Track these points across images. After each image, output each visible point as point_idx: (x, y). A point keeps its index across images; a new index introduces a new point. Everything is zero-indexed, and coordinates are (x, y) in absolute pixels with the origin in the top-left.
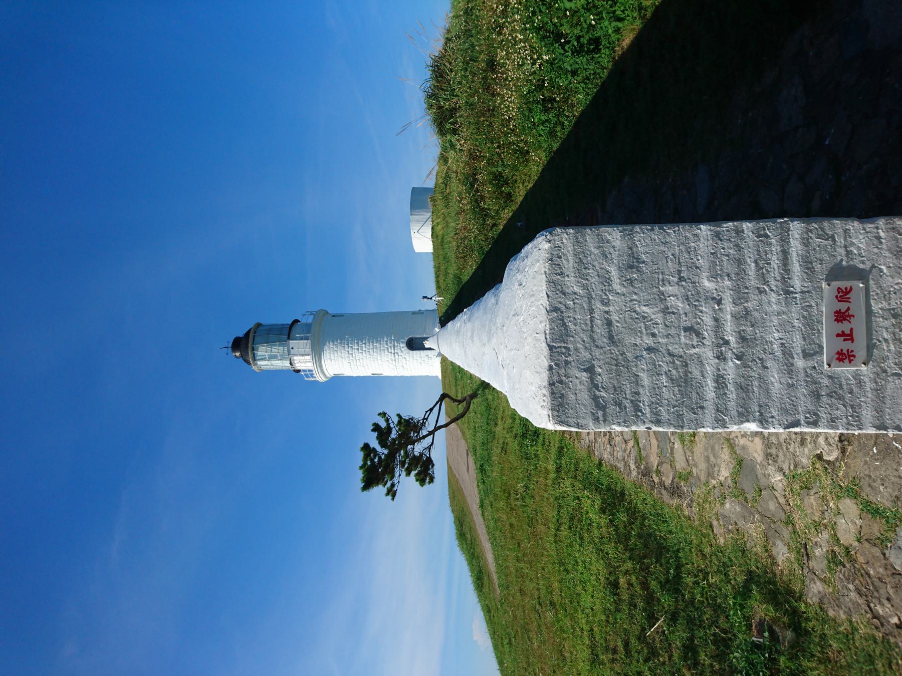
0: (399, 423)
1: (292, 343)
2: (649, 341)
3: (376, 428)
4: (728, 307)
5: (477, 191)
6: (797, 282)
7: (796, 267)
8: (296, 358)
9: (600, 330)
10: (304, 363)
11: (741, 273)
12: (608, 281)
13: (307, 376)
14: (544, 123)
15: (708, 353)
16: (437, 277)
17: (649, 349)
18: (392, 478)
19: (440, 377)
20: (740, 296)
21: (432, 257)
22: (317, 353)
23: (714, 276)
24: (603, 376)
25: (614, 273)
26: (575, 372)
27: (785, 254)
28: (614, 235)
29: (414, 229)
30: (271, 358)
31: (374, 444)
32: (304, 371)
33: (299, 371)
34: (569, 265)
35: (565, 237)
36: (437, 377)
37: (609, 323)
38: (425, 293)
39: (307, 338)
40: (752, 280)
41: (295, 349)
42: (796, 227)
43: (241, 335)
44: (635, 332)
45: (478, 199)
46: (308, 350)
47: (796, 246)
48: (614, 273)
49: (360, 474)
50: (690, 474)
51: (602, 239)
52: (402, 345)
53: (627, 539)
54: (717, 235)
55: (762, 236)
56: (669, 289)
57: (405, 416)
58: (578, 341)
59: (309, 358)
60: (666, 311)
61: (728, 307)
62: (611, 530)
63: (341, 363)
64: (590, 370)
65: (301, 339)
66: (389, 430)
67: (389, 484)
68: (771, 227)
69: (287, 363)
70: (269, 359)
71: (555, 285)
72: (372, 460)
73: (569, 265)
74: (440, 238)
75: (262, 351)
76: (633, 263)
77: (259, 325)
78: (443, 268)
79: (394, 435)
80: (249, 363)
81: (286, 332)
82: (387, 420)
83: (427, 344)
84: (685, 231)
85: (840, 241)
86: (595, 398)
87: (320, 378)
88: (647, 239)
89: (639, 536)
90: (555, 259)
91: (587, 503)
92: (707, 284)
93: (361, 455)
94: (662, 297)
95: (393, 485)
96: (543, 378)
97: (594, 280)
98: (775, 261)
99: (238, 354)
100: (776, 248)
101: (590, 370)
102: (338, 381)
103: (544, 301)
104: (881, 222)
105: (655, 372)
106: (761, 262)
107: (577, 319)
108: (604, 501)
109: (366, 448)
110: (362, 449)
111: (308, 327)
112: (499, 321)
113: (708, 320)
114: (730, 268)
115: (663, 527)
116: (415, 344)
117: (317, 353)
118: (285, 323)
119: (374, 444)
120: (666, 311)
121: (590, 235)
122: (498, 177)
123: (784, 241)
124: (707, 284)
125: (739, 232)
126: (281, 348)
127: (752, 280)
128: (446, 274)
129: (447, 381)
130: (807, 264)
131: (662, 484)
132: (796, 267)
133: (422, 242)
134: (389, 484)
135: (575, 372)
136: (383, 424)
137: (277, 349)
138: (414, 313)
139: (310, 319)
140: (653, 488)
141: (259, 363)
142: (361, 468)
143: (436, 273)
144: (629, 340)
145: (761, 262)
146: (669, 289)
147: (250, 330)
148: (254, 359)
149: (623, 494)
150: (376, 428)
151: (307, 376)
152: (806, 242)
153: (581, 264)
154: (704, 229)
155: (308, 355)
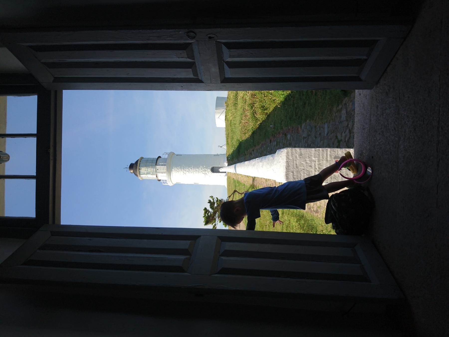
0: (217, 201)
1: (158, 167)
2: (303, 168)
3: (210, 202)
4: (317, 163)
5: (254, 110)
6: (329, 159)
7: (329, 156)
8: (158, 174)
9: (295, 166)
10: (162, 176)
11: (319, 157)
12: (296, 157)
13: (164, 183)
14: (282, 95)
15: (313, 170)
16: (227, 139)
17: (303, 169)
18: (215, 222)
19: (226, 186)
20: (319, 161)
21: (225, 130)
22: (169, 171)
23: (315, 157)
24: (295, 174)
25: (298, 156)
26: (290, 173)
27: (327, 154)
28: (298, 149)
29: (217, 116)
30: (148, 173)
31: (209, 208)
32: (163, 180)
33: (160, 180)
34: (290, 154)
35: (289, 149)
36: (224, 186)
37: (296, 164)
38: (220, 146)
39: (165, 165)
40: (321, 158)
41: (159, 170)
42: (329, 150)
43: (134, 162)
44: (301, 166)
45: (254, 113)
46: (165, 171)
47: (329, 153)
48: (298, 156)
49: (203, 219)
50: (320, 206)
51: (296, 150)
52: (209, 170)
53: (303, 227)
54: (315, 150)
55: (323, 151)
56: (307, 159)
57: (219, 199)
58: (291, 168)
59: (165, 174)
60: (306, 163)
61: (317, 163)
62: (299, 226)
63: (180, 177)
64: (293, 172)
65: (162, 165)
66: (214, 203)
67: (214, 224)
68: (325, 149)
69: (155, 176)
70: (146, 174)
71: (287, 158)
72: (208, 214)
73: (290, 154)
74: (229, 122)
75: (143, 170)
76: (301, 154)
77: (142, 158)
78: (230, 135)
79: (216, 205)
80: (137, 175)
81: (156, 161)
82: (213, 199)
83: (221, 170)
84: (310, 149)
85: (336, 152)
86: (294, 177)
87: (170, 184)
88: (303, 150)
89: (307, 226)
90: (287, 153)
91: (292, 220)
92: (314, 159)
93: (203, 212)
94: (306, 160)
95: (215, 225)
96: (285, 174)
97: (294, 157)
98: (325, 155)
99: (132, 171)
100: (325, 153)
101: (293, 172)
102: (178, 186)
103: (285, 160)
104: (344, 149)
105: (304, 173)
106: (323, 155)
107: (291, 164)
108: (297, 219)
109: (205, 209)
110: (204, 210)
111: (165, 160)
112: (275, 163)
113: (313, 165)
114: (317, 156)
115: (313, 223)
116: (214, 170)
117: (169, 171)
118: (155, 157)
119: (209, 208)
120: (306, 163)
121: (294, 149)
122: (263, 107)
123: (327, 152)
124: (314, 159)
125: (319, 150)
126: (152, 169)
127: (321, 158)
128: (233, 138)
129: (230, 187)
130: (331, 156)
131: (314, 211)
132: (329, 156)
133: (220, 121)
134: (214, 224)
135: (290, 173)
136: (212, 201)
137: (150, 170)
138: (215, 155)
139: (166, 156)
140: (311, 212)
141: (142, 176)
142: (204, 217)
143: (227, 137)
144: (300, 168)
145: (323, 155)
146: (307, 159)
147: (138, 160)
148: (140, 174)
149: (303, 216)
150: (210, 202)
151: (164, 183)
152: (330, 152)
153: (292, 154)
154: (313, 149)
155: (165, 173)
